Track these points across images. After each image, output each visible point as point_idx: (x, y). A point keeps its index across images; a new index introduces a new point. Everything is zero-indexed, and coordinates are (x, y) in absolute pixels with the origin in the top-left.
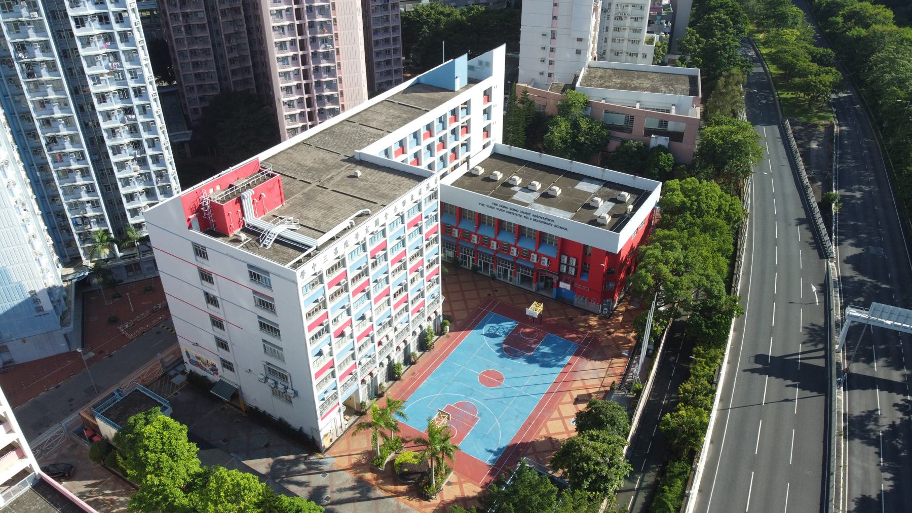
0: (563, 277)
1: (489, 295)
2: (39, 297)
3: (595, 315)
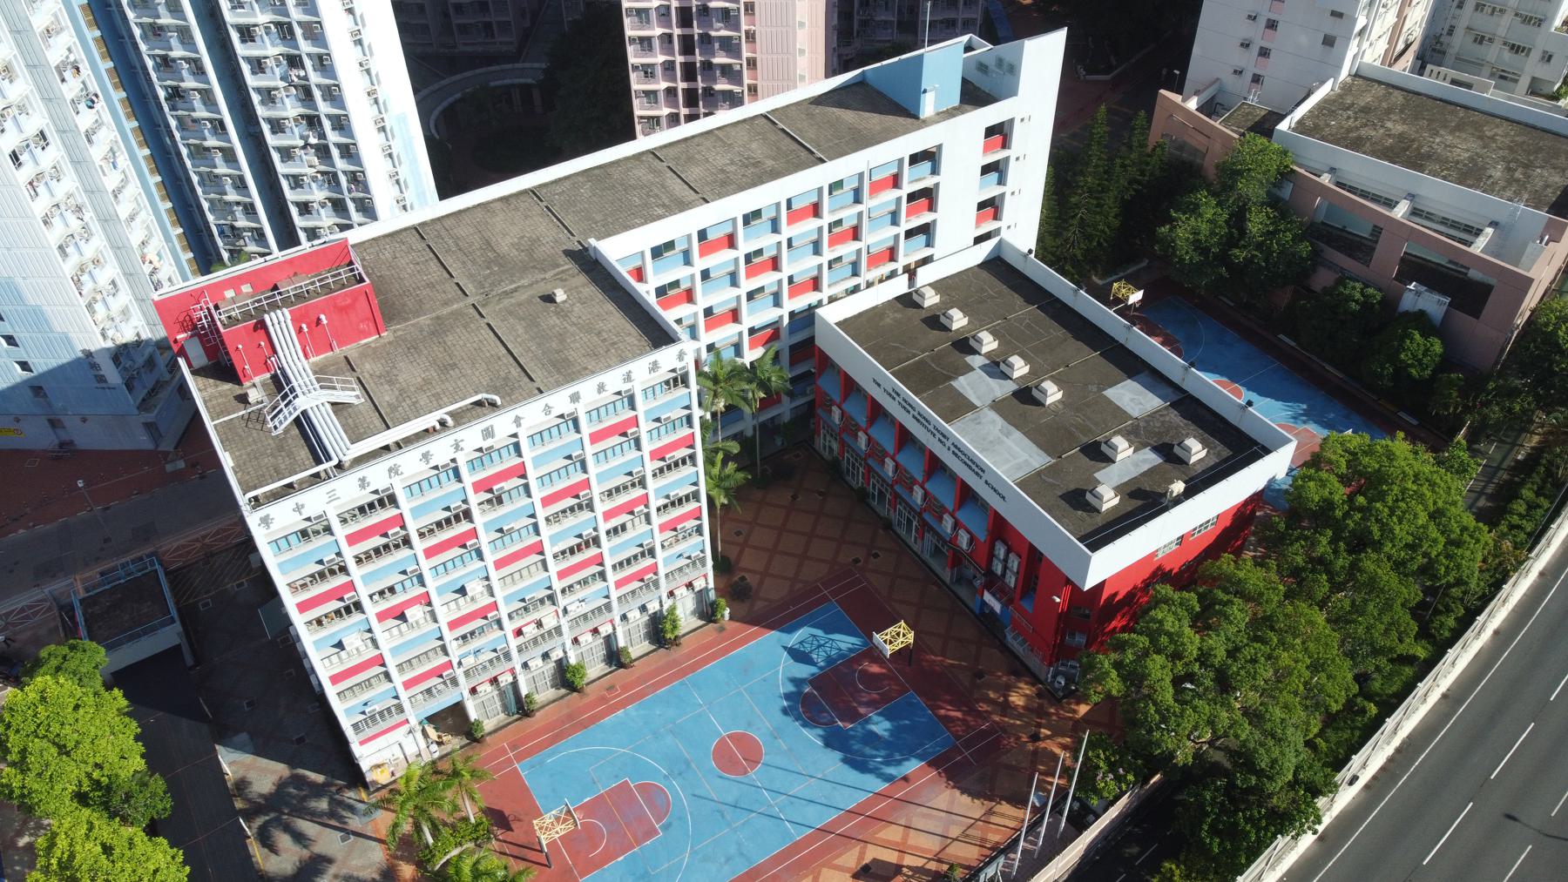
0: (994, 583)
1: (856, 561)
2: (97, 360)
3: (1034, 679)
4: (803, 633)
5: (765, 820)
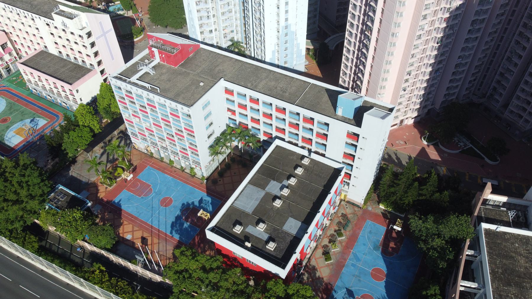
4: (209, 199)
5: (151, 214)
